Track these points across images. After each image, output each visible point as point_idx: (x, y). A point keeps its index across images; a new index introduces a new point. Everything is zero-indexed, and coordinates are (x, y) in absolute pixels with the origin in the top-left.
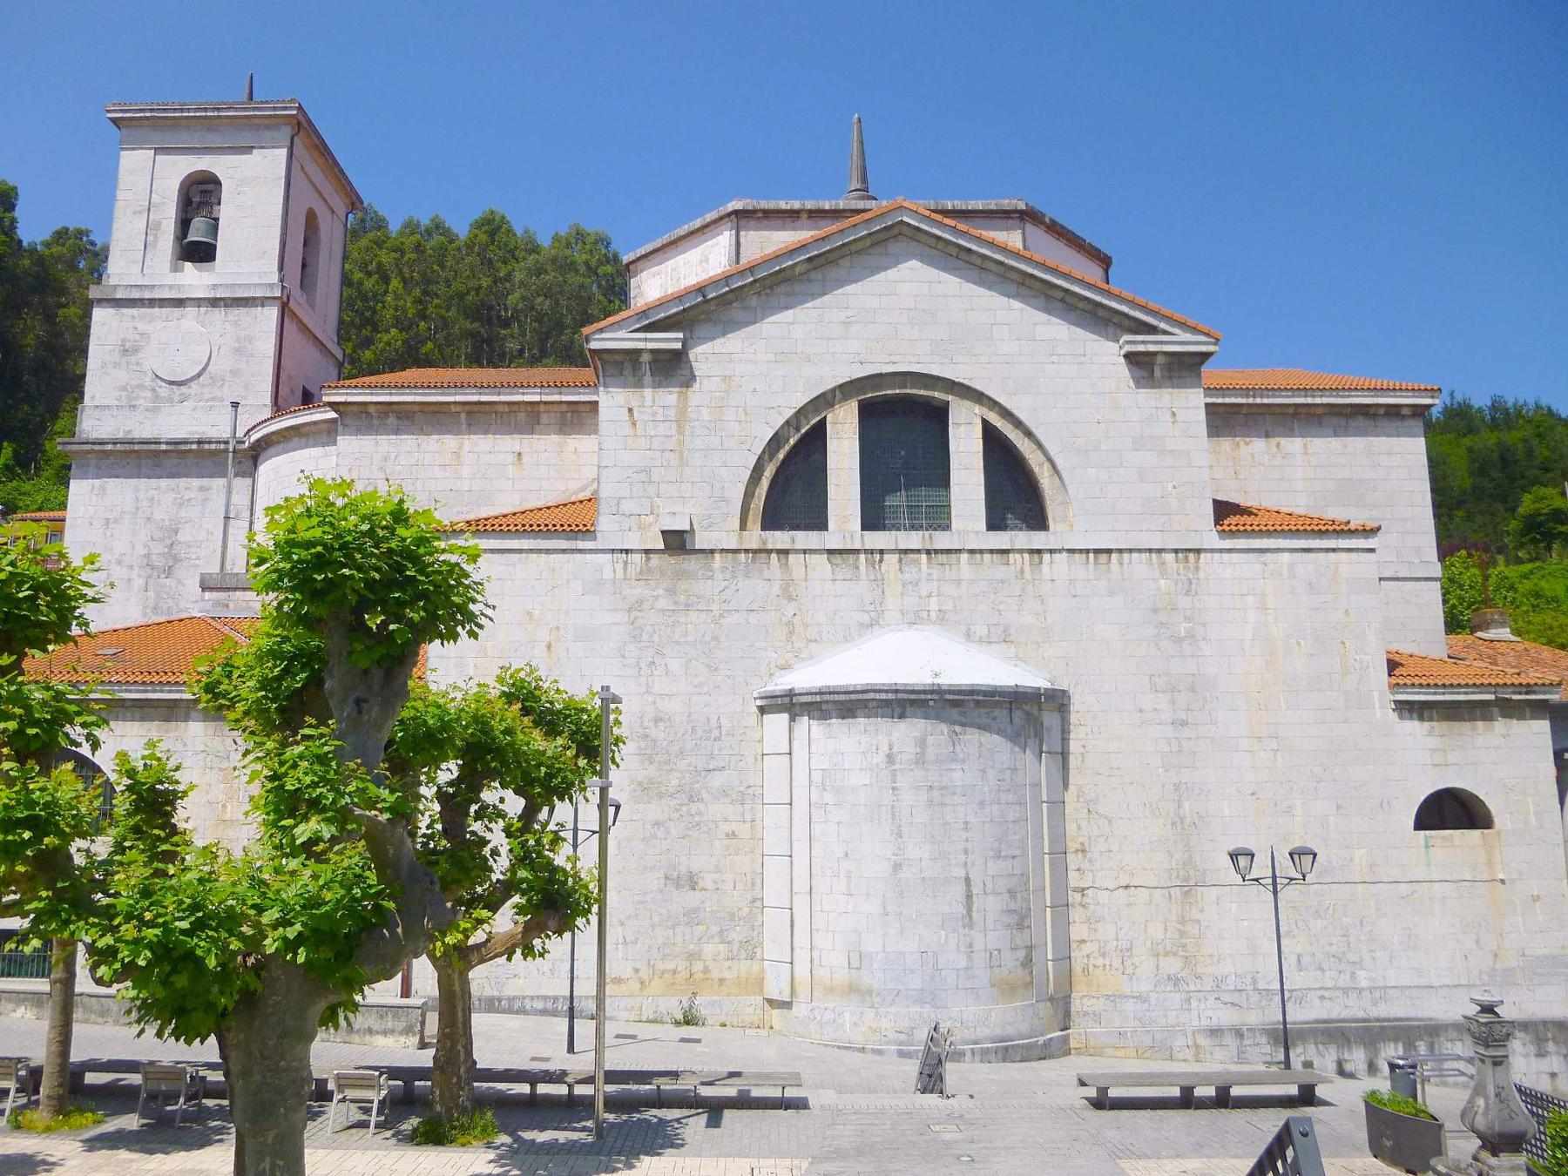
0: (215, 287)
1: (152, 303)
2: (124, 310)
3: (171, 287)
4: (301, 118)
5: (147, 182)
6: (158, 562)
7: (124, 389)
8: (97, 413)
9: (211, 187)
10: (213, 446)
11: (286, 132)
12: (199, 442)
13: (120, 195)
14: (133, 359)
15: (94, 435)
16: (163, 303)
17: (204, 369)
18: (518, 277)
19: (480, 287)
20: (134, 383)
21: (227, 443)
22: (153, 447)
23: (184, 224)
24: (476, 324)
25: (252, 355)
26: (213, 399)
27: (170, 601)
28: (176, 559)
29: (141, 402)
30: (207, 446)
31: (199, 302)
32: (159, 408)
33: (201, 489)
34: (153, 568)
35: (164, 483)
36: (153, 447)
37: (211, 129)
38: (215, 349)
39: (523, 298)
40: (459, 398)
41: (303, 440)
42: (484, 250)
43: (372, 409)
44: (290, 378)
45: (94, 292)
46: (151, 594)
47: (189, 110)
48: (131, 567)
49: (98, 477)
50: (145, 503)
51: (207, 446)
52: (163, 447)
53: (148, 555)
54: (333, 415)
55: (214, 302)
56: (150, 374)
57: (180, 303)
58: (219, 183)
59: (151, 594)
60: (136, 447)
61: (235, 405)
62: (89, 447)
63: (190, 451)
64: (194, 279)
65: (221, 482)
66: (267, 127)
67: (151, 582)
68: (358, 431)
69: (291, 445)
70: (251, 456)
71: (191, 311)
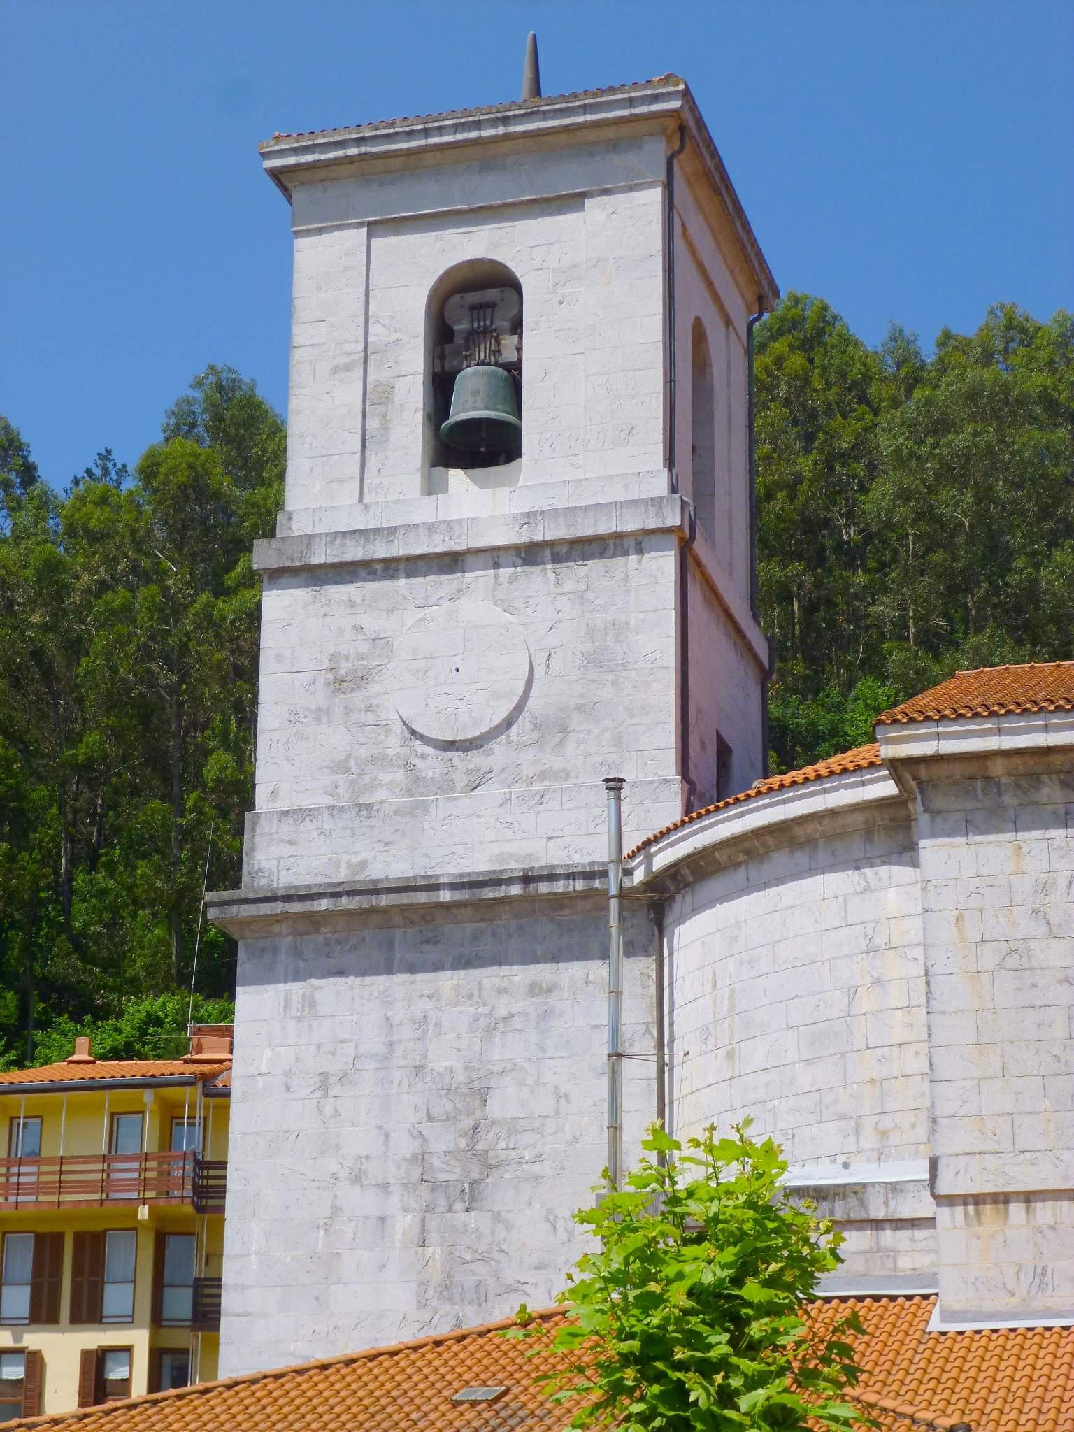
0: (530, 517)
1: (391, 568)
2: (333, 591)
3: (432, 528)
4: (687, 116)
5: (354, 303)
6: (449, 1174)
7: (341, 767)
8: (286, 828)
9: (492, 294)
10: (559, 887)
11: (657, 150)
12: (527, 879)
13: (301, 334)
14: (357, 698)
15: (286, 879)
16: (414, 565)
17: (519, 708)
18: (886, 444)
19: (798, 479)
20: (364, 752)
21: (604, 874)
22: (422, 897)
23: (441, 386)
24: (796, 567)
25: (624, 667)
26: (542, 776)
27: (479, 1268)
28: (488, 1164)
29: (381, 795)
30: (544, 888)
31: (494, 556)
32: (424, 807)
33: (534, 989)
34: (435, 1186)
35: (448, 981)
36: (422, 897)
37: (487, 166)
38: (539, 660)
39: (905, 495)
40: (1007, 743)
41: (802, 858)
42: (800, 391)
43: (997, 768)
44: (699, 711)
45: (263, 555)
46: (434, 1251)
47: (440, 130)
48: (385, 1187)
49: (297, 976)
50: (407, 1032)
51: (544, 888)
52: (445, 896)
53: (421, 1158)
54: (889, 788)
55: (529, 554)
56: (398, 728)
57: (452, 562)
58: (517, 288)
59: (434, 1251)
60: (384, 901)
61: (614, 785)
62: (278, 908)
63: (507, 900)
64: (476, 506)
65: (598, 970)
66: (614, 146)
67: (433, 1223)
68: (969, 826)
69: (767, 869)
70: (659, 902)
71: (478, 578)
